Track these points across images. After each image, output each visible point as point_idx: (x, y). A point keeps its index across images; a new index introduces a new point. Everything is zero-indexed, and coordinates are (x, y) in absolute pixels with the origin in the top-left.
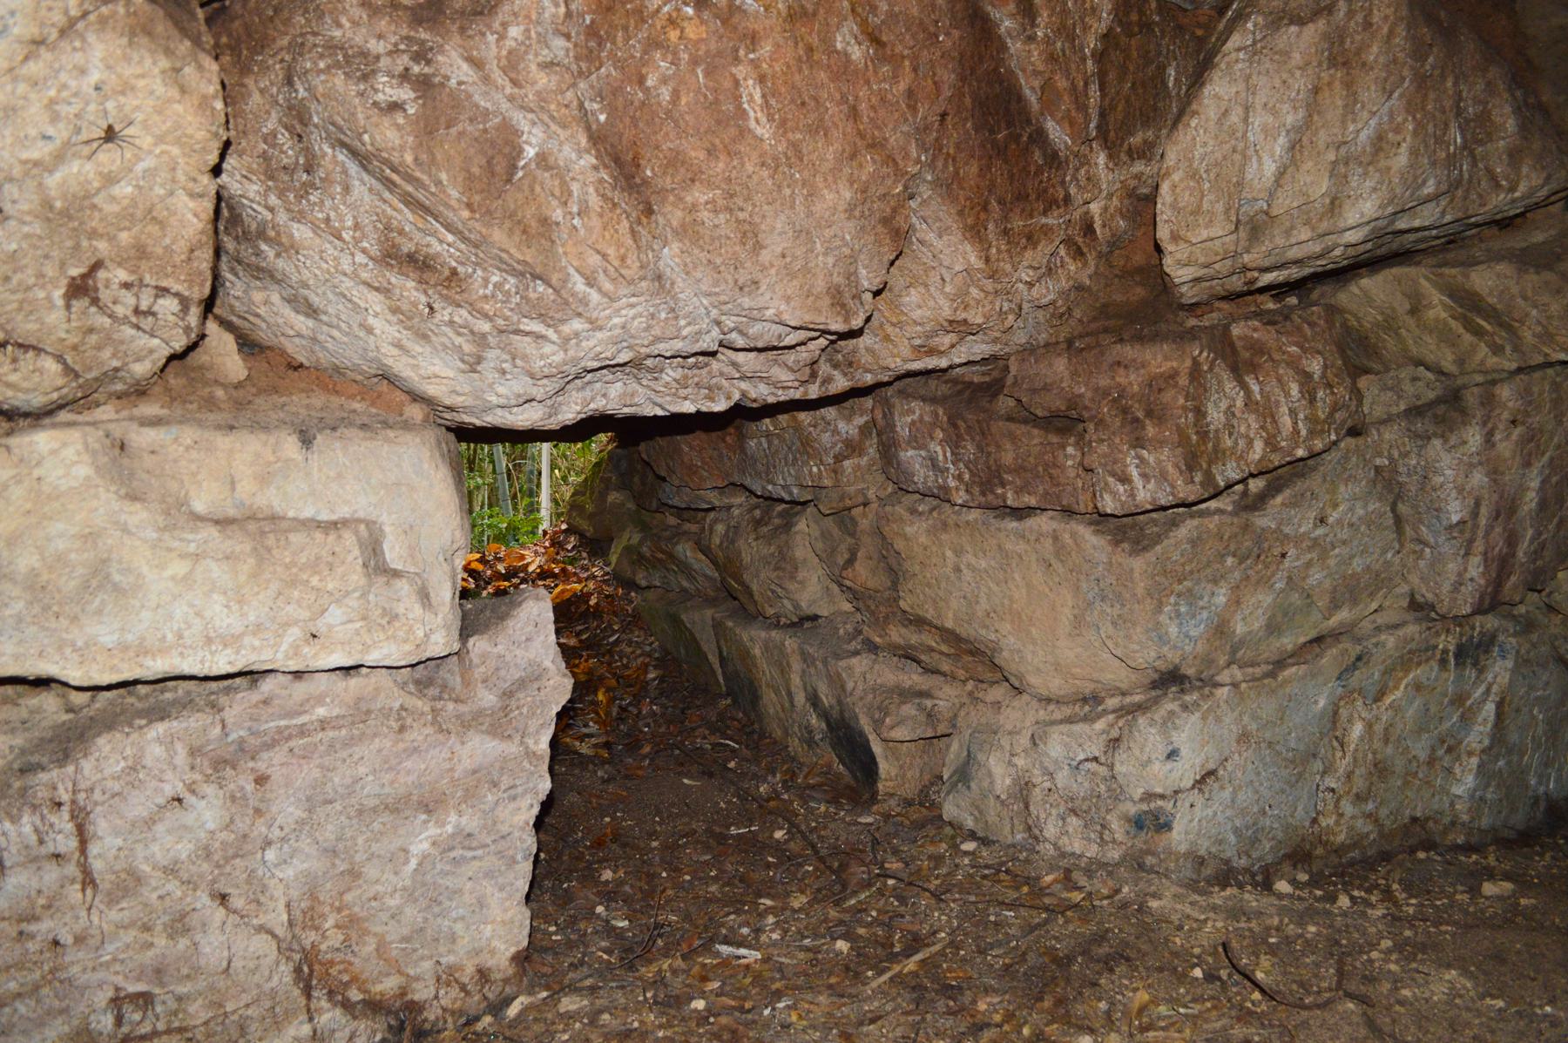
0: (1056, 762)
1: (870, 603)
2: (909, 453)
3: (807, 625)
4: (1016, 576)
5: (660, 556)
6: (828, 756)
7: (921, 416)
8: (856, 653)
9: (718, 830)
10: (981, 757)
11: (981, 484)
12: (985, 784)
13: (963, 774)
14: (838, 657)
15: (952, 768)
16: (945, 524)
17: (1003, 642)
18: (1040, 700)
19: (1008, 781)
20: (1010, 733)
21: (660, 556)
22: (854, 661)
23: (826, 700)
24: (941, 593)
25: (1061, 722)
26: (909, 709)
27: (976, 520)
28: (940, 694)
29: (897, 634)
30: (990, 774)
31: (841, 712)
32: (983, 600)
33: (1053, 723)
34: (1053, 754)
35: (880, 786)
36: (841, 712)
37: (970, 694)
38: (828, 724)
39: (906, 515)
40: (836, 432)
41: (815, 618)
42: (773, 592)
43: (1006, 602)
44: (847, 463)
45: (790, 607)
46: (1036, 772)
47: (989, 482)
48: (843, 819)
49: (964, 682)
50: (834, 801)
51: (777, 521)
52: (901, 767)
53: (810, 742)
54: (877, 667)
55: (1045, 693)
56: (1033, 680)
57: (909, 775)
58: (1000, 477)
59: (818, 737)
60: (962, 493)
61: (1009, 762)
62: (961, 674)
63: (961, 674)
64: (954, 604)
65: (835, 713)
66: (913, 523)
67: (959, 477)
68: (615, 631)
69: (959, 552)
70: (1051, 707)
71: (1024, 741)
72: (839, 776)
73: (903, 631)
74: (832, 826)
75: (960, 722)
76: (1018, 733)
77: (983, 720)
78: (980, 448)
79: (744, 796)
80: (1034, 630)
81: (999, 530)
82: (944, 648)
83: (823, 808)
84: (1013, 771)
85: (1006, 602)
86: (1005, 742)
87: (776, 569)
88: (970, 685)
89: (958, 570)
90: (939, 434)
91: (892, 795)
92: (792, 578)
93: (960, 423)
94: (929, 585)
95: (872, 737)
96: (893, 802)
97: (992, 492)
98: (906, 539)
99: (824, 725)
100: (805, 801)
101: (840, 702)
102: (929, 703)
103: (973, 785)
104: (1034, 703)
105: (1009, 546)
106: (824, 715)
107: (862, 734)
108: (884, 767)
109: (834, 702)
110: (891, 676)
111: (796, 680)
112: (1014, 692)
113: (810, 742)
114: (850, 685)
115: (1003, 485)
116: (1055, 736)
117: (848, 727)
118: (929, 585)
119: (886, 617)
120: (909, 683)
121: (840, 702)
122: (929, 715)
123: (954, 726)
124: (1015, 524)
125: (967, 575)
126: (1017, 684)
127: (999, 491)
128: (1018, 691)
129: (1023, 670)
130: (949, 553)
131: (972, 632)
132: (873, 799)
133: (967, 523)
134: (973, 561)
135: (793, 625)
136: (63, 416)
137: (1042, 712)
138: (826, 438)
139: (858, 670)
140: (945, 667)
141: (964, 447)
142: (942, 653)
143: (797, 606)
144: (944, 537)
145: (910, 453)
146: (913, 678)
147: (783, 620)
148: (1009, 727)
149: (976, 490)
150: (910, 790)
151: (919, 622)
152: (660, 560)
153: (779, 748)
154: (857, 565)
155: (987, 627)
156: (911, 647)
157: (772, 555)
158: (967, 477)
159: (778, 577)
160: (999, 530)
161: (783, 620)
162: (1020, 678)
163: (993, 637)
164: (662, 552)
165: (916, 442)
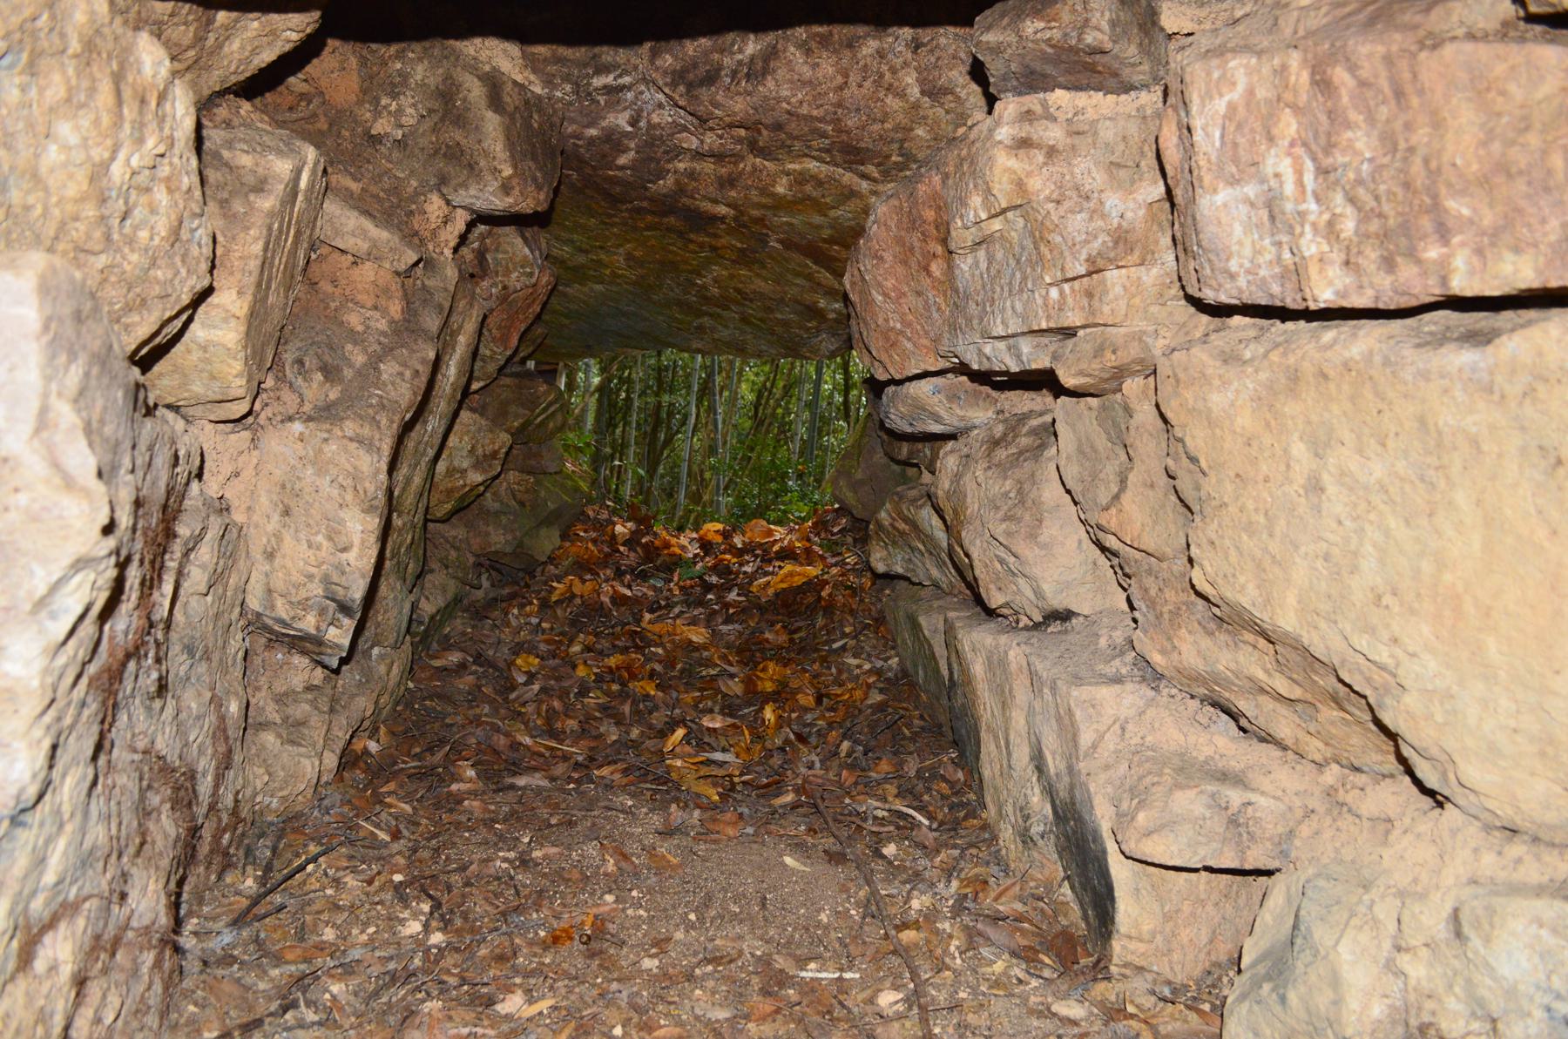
0: (1511, 993)
1: (1150, 582)
2: (1220, 198)
3: (1055, 627)
4: (1460, 497)
5: (902, 526)
6: (1049, 864)
7: (1250, 92)
8: (1117, 680)
9: (780, 962)
10: (1321, 934)
11: (1385, 236)
12: (1323, 1001)
13: (1279, 966)
14: (1078, 680)
15: (1264, 944)
16: (1295, 377)
17: (1409, 672)
18: (1488, 828)
19: (1377, 1010)
20: (1402, 894)
21: (902, 526)
22: (1105, 693)
23: (1054, 764)
24: (1274, 547)
25: (1539, 891)
26: (1190, 802)
27: (1369, 356)
28: (1265, 783)
29: (1195, 648)
30: (1335, 981)
31: (1072, 787)
32: (1368, 564)
33: (1516, 890)
34: (1505, 970)
35: (1116, 945)
36: (1072, 787)
37: (1330, 792)
38: (1055, 812)
39: (1213, 366)
40: (1098, 212)
41: (1065, 616)
42: (1002, 562)
43: (1427, 566)
44: (1112, 275)
45: (1029, 593)
46: (1452, 1004)
47: (1405, 228)
48: (1025, 999)
49: (1320, 766)
50: (1027, 956)
51: (1024, 441)
52: (1167, 917)
53: (1026, 838)
54: (1151, 713)
55: (1506, 812)
56: (1472, 772)
57: (1185, 935)
58: (1436, 207)
59: (1036, 829)
60: (1335, 271)
61: (1391, 967)
62: (1315, 748)
63: (1315, 748)
64: (1300, 572)
65: (1063, 794)
66: (1225, 383)
67: (1331, 230)
68: (844, 635)
69: (1318, 449)
70: (1518, 849)
71: (1432, 919)
72: (1059, 908)
73: (1205, 642)
74: (998, 1006)
75: (1298, 848)
76: (1423, 896)
77: (1348, 854)
78: (1389, 142)
79: (874, 908)
80: (1492, 645)
81: (1425, 376)
82: (1281, 685)
83: (999, 967)
84: (1396, 986)
85: (1427, 566)
86: (1386, 911)
87: (1007, 518)
88: (1332, 774)
89: (1315, 487)
90: (1289, 126)
91: (1140, 969)
92: (1032, 536)
93: (1340, 75)
94: (1250, 528)
95: (1111, 847)
96: (1139, 985)
97: (1412, 255)
98: (1211, 423)
99: (1048, 810)
100: (973, 939)
101: (1070, 769)
102: (1235, 797)
103: (1292, 996)
104: (1474, 829)
105: (1446, 418)
106: (1050, 792)
107: (1097, 838)
108: (1126, 910)
109: (1062, 766)
110: (1174, 733)
111: (1019, 719)
112: (1427, 802)
113: (1026, 838)
114: (1086, 738)
115: (1443, 233)
116: (1518, 925)
117: (1079, 820)
118: (1250, 528)
119: (1176, 613)
120: (1207, 751)
121: (1070, 769)
122: (1233, 822)
123: (1284, 854)
124: (1466, 357)
125: (1336, 499)
126: (1432, 782)
127: (1433, 253)
128: (270, 591)
129: (1450, 744)
130: (1299, 449)
131: (1337, 644)
132: (1100, 969)
133: (1347, 366)
134: (1354, 465)
135: (1036, 626)
136: (970, 578)
137: (1488, 859)
138: (1077, 224)
139: (1109, 711)
140: (1285, 725)
141: (1350, 147)
142: (1280, 698)
143: (1039, 593)
144: (1291, 408)
145: (1223, 195)
146: (1220, 741)
147: (1024, 621)
148: (1402, 879)
149: (1370, 257)
150: (1184, 966)
151: (1229, 620)
152: (902, 534)
153: (989, 834)
154: (1126, 499)
155: (1371, 630)
156: (1217, 679)
157: (1006, 495)
158: (1348, 226)
159: (1009, 534)
160: (1425, 376)
161: (1024, 621)
162: (1446, 763)
163: (1383, 655)
164: (906, 520)
165: (1241, 167)
